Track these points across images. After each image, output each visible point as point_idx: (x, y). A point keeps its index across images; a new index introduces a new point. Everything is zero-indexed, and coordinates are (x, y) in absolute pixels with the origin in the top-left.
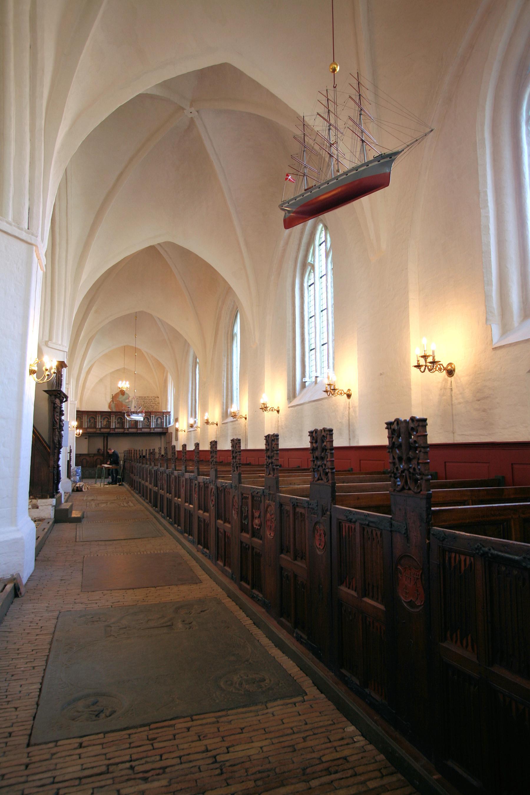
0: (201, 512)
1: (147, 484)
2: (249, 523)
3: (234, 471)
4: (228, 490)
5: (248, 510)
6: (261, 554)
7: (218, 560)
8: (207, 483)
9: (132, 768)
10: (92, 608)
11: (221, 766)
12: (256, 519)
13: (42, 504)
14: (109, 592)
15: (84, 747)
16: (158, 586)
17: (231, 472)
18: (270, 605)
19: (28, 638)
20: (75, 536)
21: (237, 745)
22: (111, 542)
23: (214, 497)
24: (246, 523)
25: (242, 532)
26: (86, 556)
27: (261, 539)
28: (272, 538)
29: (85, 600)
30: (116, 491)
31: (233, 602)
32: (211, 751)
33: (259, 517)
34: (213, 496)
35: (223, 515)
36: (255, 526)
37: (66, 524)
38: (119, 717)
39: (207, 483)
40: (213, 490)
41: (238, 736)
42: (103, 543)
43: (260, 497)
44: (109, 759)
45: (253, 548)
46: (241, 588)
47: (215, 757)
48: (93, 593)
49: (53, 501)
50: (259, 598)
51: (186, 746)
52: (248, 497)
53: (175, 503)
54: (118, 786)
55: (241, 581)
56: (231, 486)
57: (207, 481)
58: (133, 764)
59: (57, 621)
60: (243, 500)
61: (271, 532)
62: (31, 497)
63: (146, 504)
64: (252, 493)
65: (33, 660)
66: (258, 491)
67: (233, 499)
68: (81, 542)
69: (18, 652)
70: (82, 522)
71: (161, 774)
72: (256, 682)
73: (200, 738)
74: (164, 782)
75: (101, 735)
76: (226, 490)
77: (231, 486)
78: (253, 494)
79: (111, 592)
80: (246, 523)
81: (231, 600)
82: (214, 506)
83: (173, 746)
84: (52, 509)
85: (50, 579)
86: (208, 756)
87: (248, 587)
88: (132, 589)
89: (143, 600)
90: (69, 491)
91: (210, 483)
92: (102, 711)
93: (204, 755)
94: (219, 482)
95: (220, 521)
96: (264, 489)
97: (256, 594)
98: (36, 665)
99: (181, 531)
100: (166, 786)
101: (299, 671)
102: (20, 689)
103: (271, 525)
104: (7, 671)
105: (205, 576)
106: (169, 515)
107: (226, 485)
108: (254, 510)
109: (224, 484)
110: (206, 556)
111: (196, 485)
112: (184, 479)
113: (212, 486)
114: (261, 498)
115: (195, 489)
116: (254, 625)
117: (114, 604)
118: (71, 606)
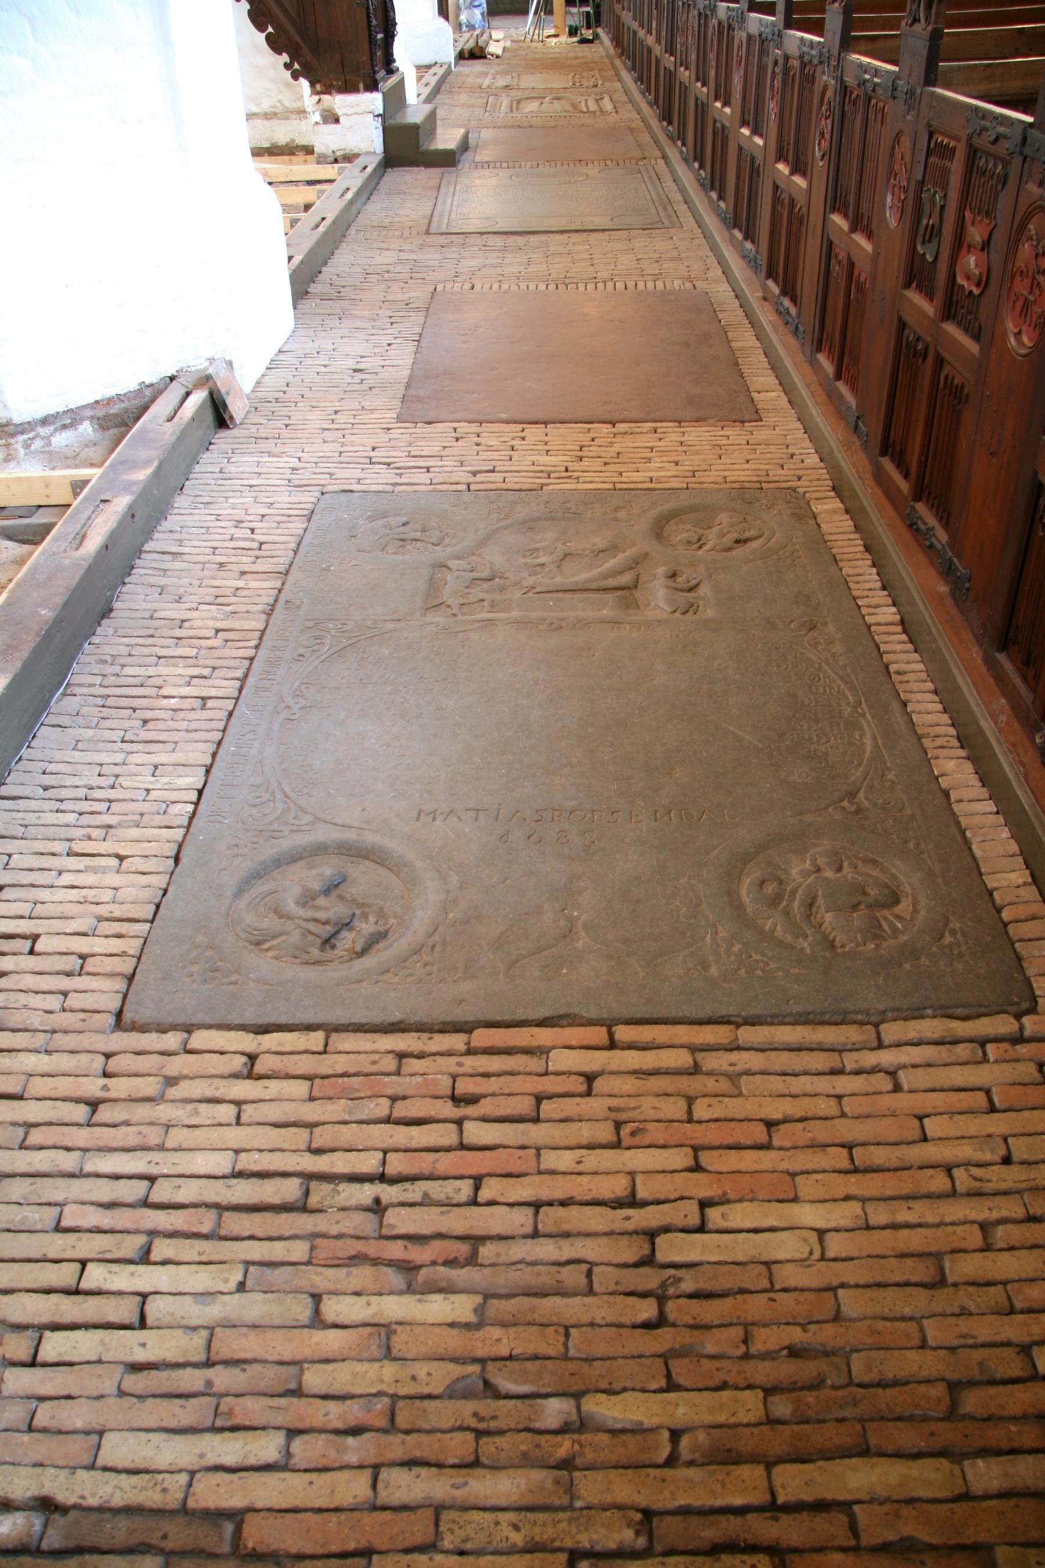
0: (783, 168)
1: (650, 40)
2: (939, 259)
3: (916, 20)
4: (880, 105)
5: (942, 208)
6: (967, 395)
7: (819, 350)
8: (810, 61)
9: (378, 1207)
10: (409, 488)
11: (663, 1285)
12: (969, 251)
13: (346, 111)
14: (474, 428)
15: (260, 1077)
16: (622, 422)
17: (903, 24)
18: (967, 585)
19: (217, 583)
20: (430, 213)
21: (740, 1200)
22: (520, 240)
23: (829, 121)
24: (929, 258)
25: (907, 286)
26: (440, 288)
27: (976, 337)
28: (1023, 352)
29: (400, 454)
30: (576, 58)
31: (848, 517)
32: (644, 1204)
33: (986, 246)
34: (827, 118)
35: (852, 199)
36: (960, 280)
37: (416, 169)
38: (387, 971)
39: (810, 61)
40: (830, 93)
41: (748, 1160)
42: (498, 241)
43: (1003, 160)
44: (319, 1151)
45: (940, 361)
46: (879, 477)
47: (652, 1235)
48: (429, 428)
49: (374, 101)
50: (933, 540)
51: (565, 1160)
52: (954, 149)
53: (715, 121)
54: (321, 1278)
55: (883, 454)
56: (895, 89)
57: (813, 52)
58: (389, 1193)
59: (305, 525)
60: (932, 159)
61: (1024, 328)
62: (318, 87)
63: (646, 108)
64: (970, 138)
65: (206, 672)
66: (1001, 130)
67: (893, 148)
68: (441, 234)
69: (178, 633)
70: (460, 166)
71: (463, 1267)
72: (862, 906)
73: (618, 1134)
74: (462, 1307)
75: (316, 1040)
76: (873, 102)
77: (895, 89)
78: (977, 141)
79: (479, 430)
80: (929, 258)
81: (841, 505)
82: (827, 157)
83: (523, 1147)
84: (374, 123)
85: (325, 366)
86: (630, 1226)
87: (904, 486)
88: (542, 423)
89: (567, 470)
90: (445, 60)
91: (821, 63)
92: (347, 924)
93: (615, 1219)
94: (853, 62)
95: (837, 219)
96: (1030, 125)
97: (925, 524)
98: (213, 692)
99: (725, 218)
100: (467, 1326)
101: (1025, 884)
102: (147, 781)
103: (1031, 298)
104: (135, 703)
105: (774, 394)
106: (698, 156)
107: (875, 80)
108: (967, 214)
109: (867, 77)
110: (787, 323)
111: (776, 63)
112: (744, 35)
113: (825, 78)
114: (1006, 163)
115: (773, 81)
116: (899, 629)
117: (480, 478)
118: (358, 473)
